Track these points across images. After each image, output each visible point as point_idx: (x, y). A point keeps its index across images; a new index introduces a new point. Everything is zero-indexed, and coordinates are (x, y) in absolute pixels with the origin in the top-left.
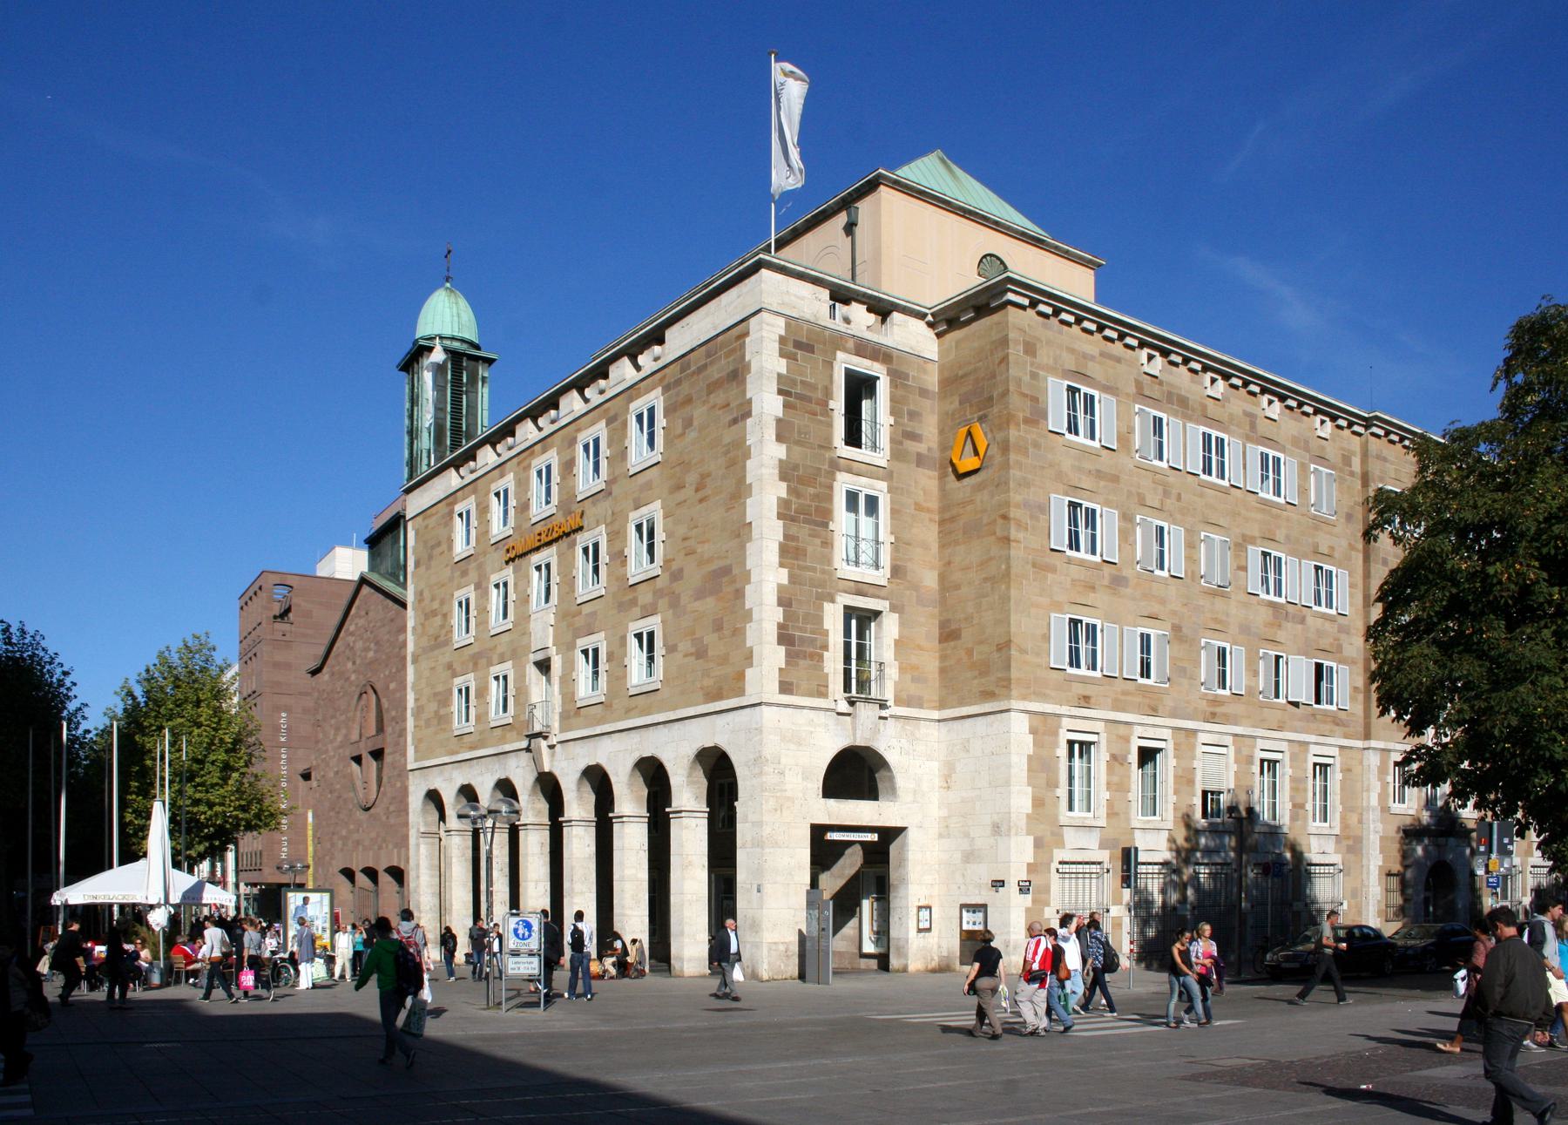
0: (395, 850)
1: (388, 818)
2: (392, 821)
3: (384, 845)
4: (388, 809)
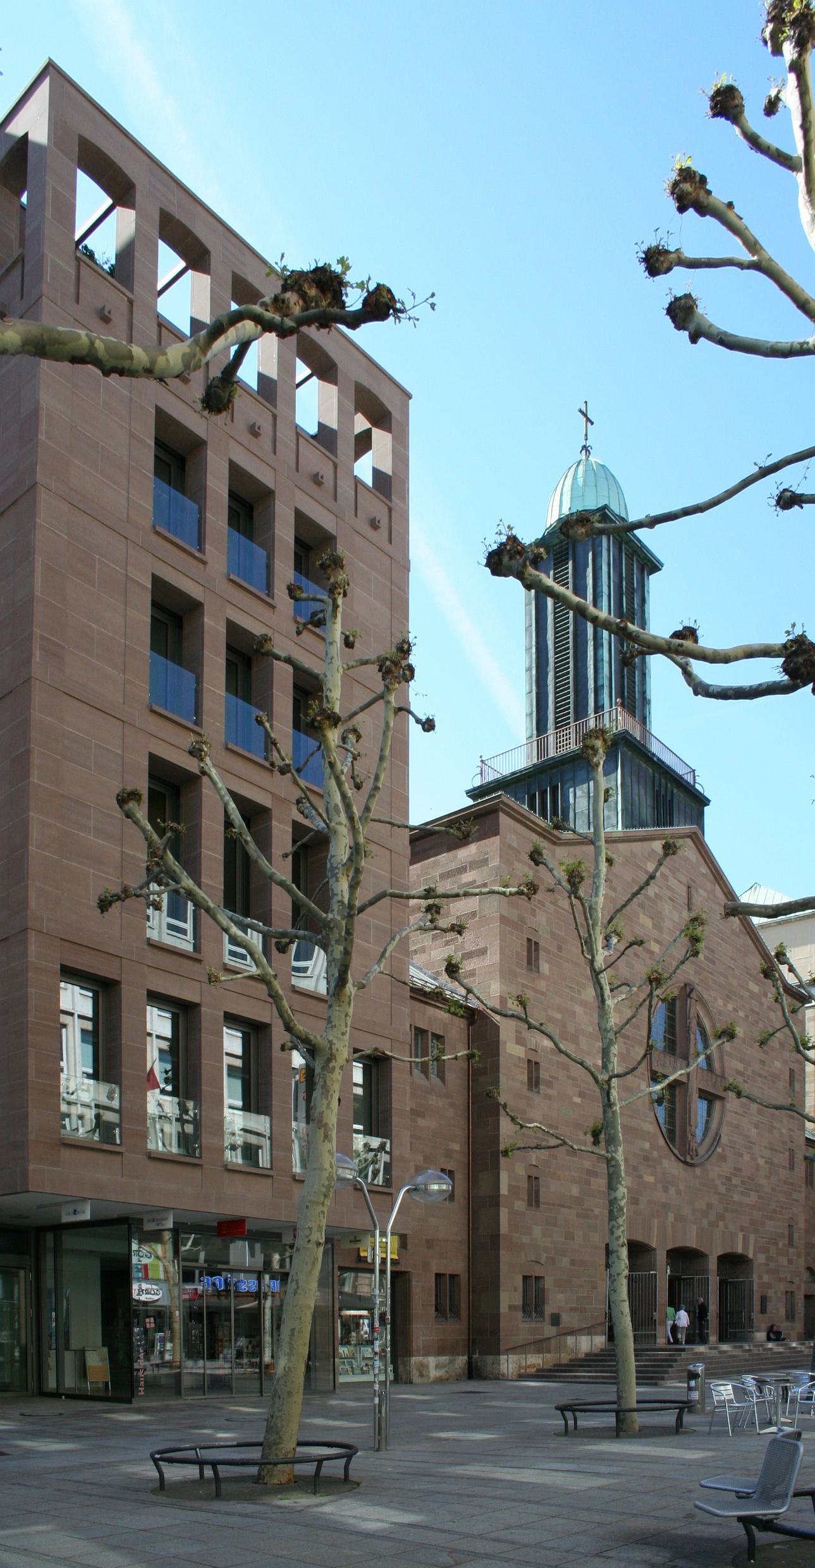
0: (740, 1235)
1: (728, 1190)
2: (736, 1197)
3: (721, 1223)
4: (729, 1179)
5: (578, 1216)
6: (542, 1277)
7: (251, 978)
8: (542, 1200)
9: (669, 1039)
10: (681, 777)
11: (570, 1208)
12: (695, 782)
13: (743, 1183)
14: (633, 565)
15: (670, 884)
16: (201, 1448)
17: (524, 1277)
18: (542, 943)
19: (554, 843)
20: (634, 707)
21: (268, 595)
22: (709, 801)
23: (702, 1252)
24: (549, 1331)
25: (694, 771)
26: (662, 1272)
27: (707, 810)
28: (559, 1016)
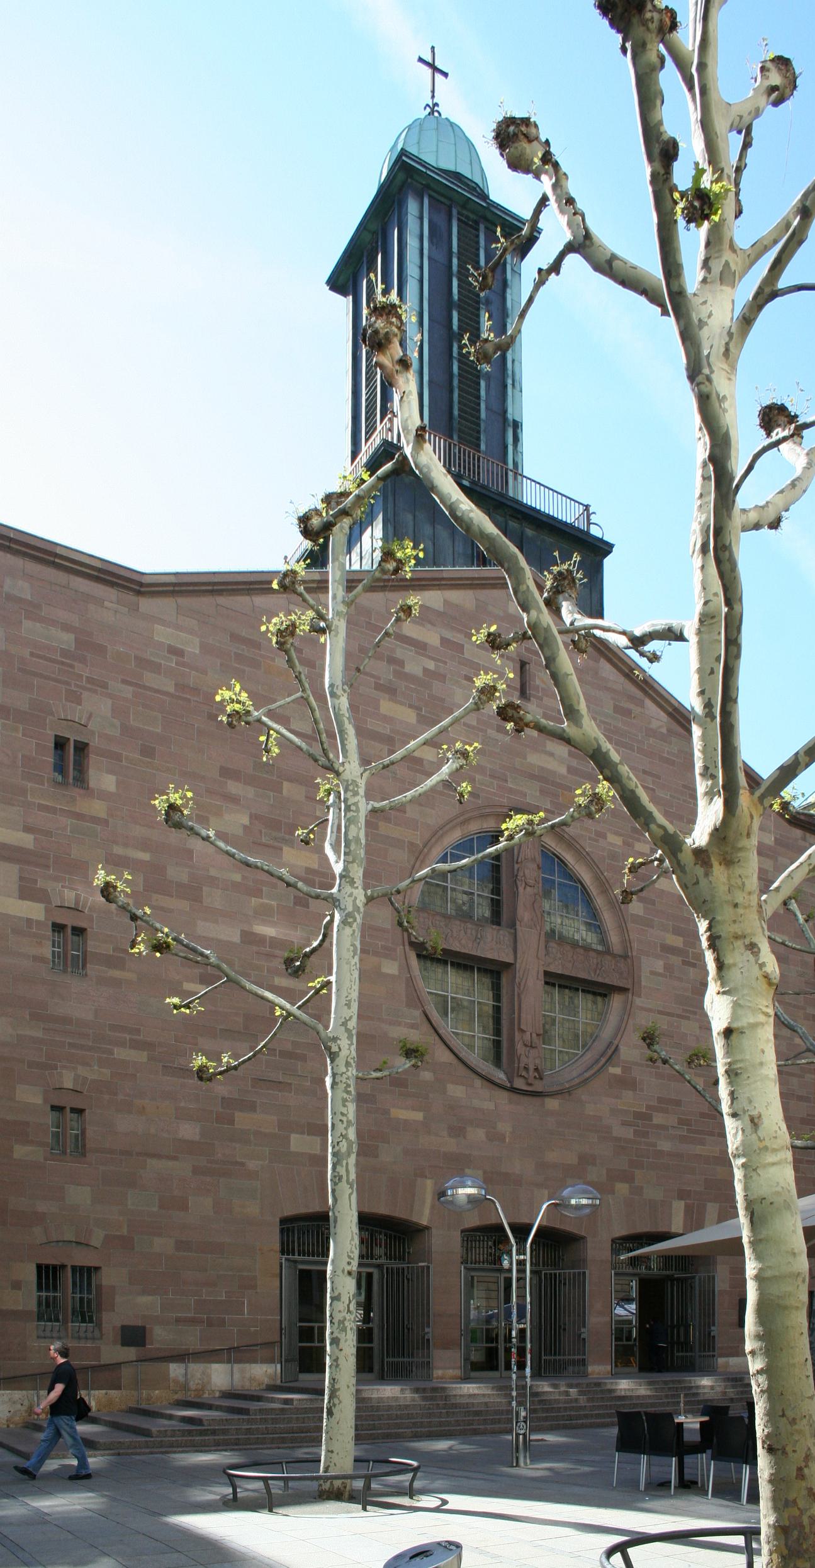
5: (196, 1171)
6: (97, 1269)
7: (766, 977)
8: (90, 1145)
9: (492, 899)
10: (571, 526)
11: (175, 1158)
12: (589, 524)
13: (681, 1122)
14: (478, 236)
15: (466, 655)
16: (287, 1462)
17: (39, 1267)
18: (95, 743)
19: (139, 593)
20: (479, 432)
21: (348, 497)
22: (611, 546)
23: (575, 1235)
24: (113, 1352)
25: (587, 507)
26: (365, 1261)
27: (607, 562)
28: (145, 856)
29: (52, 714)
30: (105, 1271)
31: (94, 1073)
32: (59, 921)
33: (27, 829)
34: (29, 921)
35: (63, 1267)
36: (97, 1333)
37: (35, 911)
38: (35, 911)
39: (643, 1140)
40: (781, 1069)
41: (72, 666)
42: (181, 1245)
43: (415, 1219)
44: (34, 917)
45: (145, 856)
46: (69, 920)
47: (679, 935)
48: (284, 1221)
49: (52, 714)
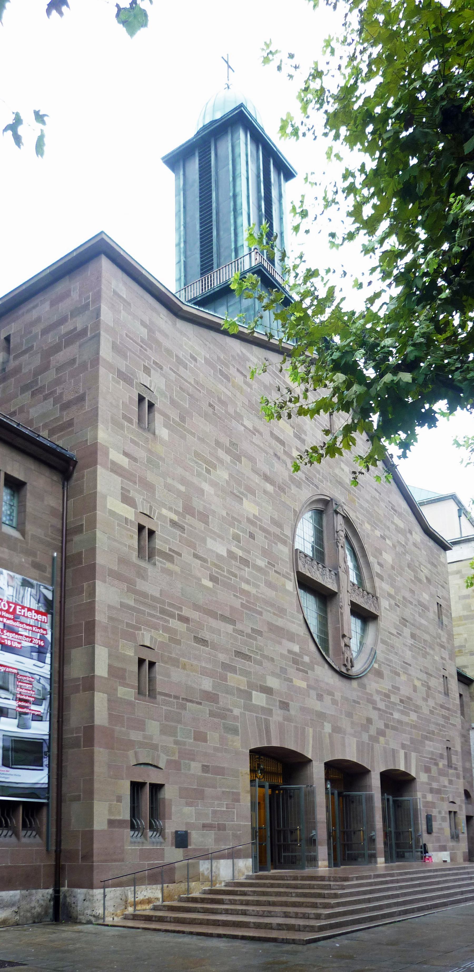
6: (161, 786)
11: (200, 704)
13: (402, 701)
28: (182, 488)
29: (137, 379)
30: (166, 787)
31: (162, 637)
32: (142, 523)
33: (126, 454)
34: (126, 519)
35: (144, 784)
36: (161, 839)
37: (128, 512)
38: (128, 512)
39: (202, 647)
40: (5, 737)
41: (146, 350)
42: (205, 769)
43: (305, 754)
44: (129, 518)
45: (182, 488)
46: (148, 524)
47: (393, 588)
48: (252, 751)
49: (137, 379)
